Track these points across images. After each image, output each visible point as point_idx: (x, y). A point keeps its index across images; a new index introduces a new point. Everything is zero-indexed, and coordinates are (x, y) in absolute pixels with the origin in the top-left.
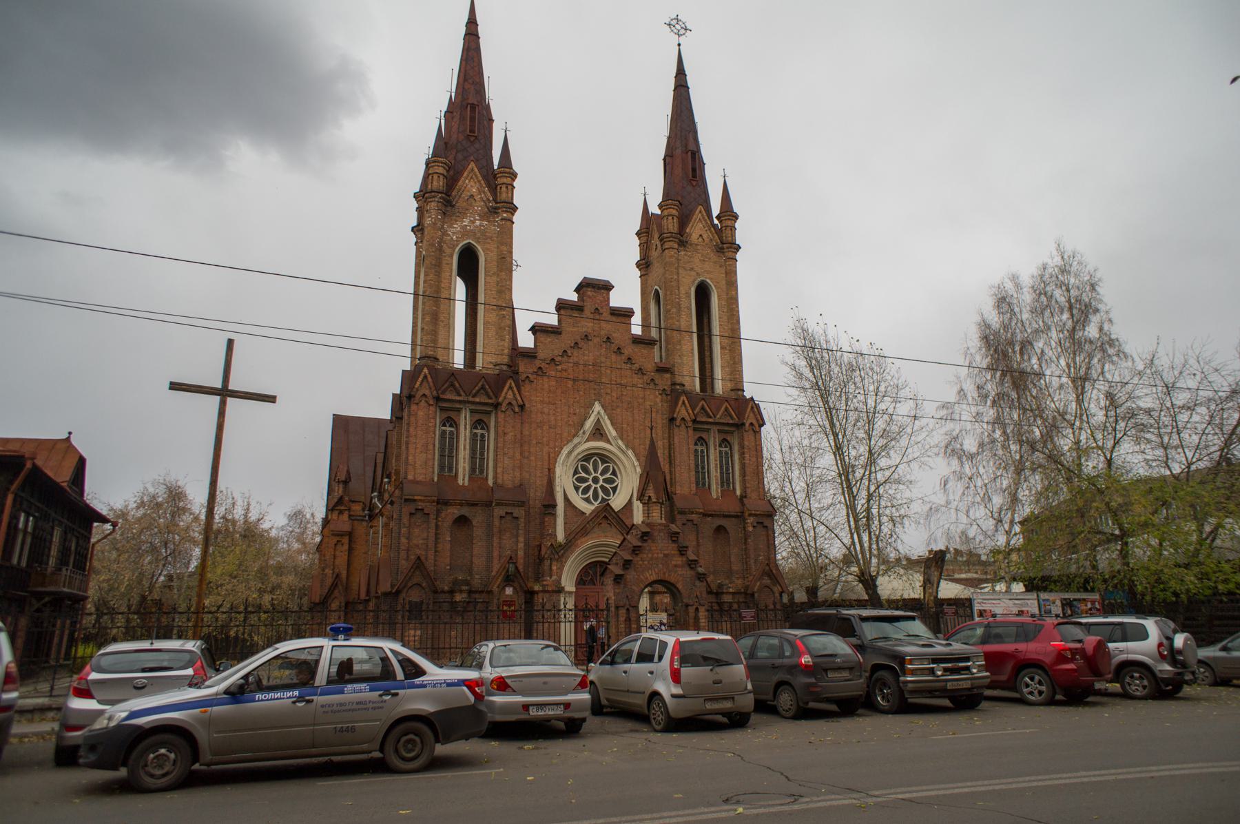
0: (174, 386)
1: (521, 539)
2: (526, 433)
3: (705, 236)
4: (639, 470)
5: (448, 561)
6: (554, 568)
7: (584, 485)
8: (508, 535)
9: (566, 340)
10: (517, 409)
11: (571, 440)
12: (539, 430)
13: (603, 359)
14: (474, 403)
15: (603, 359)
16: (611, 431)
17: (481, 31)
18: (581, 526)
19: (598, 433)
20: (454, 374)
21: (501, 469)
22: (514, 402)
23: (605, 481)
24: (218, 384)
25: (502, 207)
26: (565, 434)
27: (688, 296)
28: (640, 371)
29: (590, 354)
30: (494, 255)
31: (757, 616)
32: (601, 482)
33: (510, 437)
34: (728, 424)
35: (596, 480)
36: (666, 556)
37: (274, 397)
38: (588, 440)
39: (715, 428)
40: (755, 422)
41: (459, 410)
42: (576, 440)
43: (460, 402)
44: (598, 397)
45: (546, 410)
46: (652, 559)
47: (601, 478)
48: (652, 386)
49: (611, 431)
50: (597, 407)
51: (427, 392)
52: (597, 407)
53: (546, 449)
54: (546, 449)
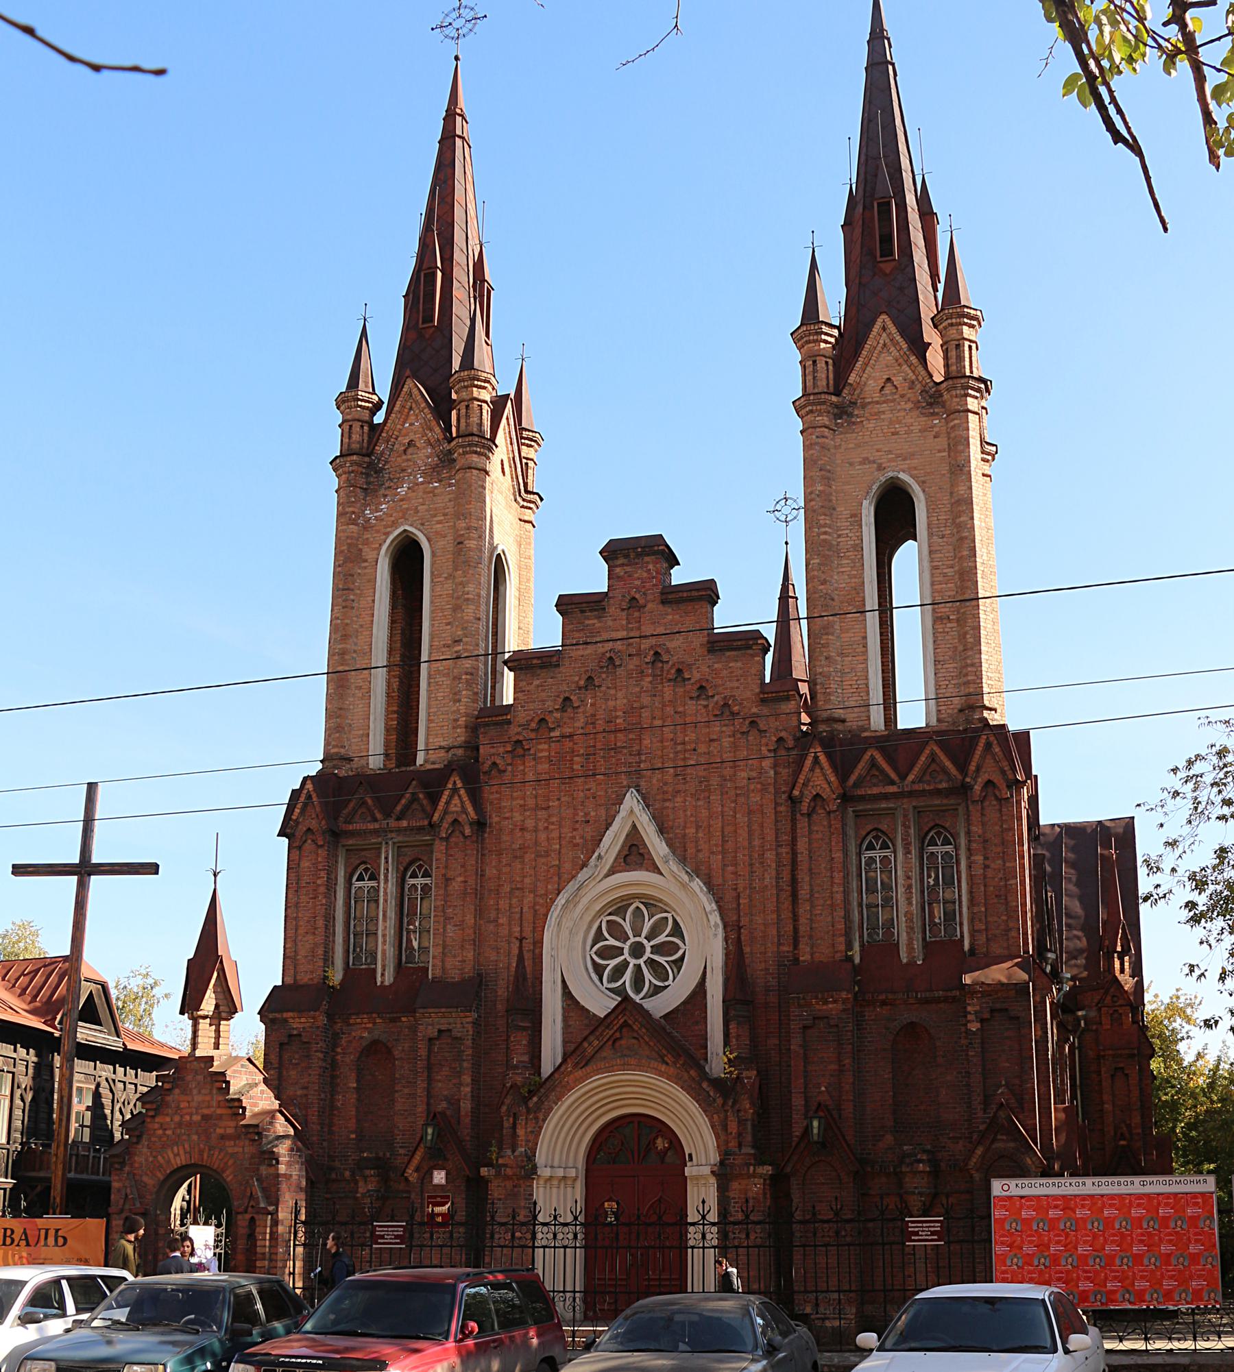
0: (153, 869)
1: (467, 1079)
2: (490, 872)
3: (898, 380)
4: (715, 918)
5: (352, 1124)
6: (520, 1132)
7: (613, 963)
8: (446, 1071)
9: (569, 676)
10: (468, 831)
11: (574, 877)
12: (517, 865)
13: (646, 700)
14: (399, 831)
15: (646, 700)
16: (658, 847)
17: (897, 53)
18: (596, 1040)
19: (634, 854)
20: (899, 744)
21: (444, 952)
22: (462, 818)
23: (656, 949)
24: (76, 860)
25: (949, 398)
26: (568, 866)
27: (856, 518)
28: (726, 710)
29: (615, 698)
30: (447, 543)
31: (407, 1237)
32: (648, 954)
33: (456, 885)
34: (938, 792)
35: (637, 950)
36: (206, 1118)
37: (157, 866)
38: (612, 872)
39: (908, 804)
40: (997, 778)
41: (891, 813)
42: (582, 876)
43: (376, 832)
44: (635, 779)
45: (530, 823)
46: (180, 1125)
47: (648, 946)
48: (754, 732)
49: (658, 847)
50: (631, 801)
51: (314, 824)
52: (631, 801)
53: (529, 898)
54: (529, 898)
